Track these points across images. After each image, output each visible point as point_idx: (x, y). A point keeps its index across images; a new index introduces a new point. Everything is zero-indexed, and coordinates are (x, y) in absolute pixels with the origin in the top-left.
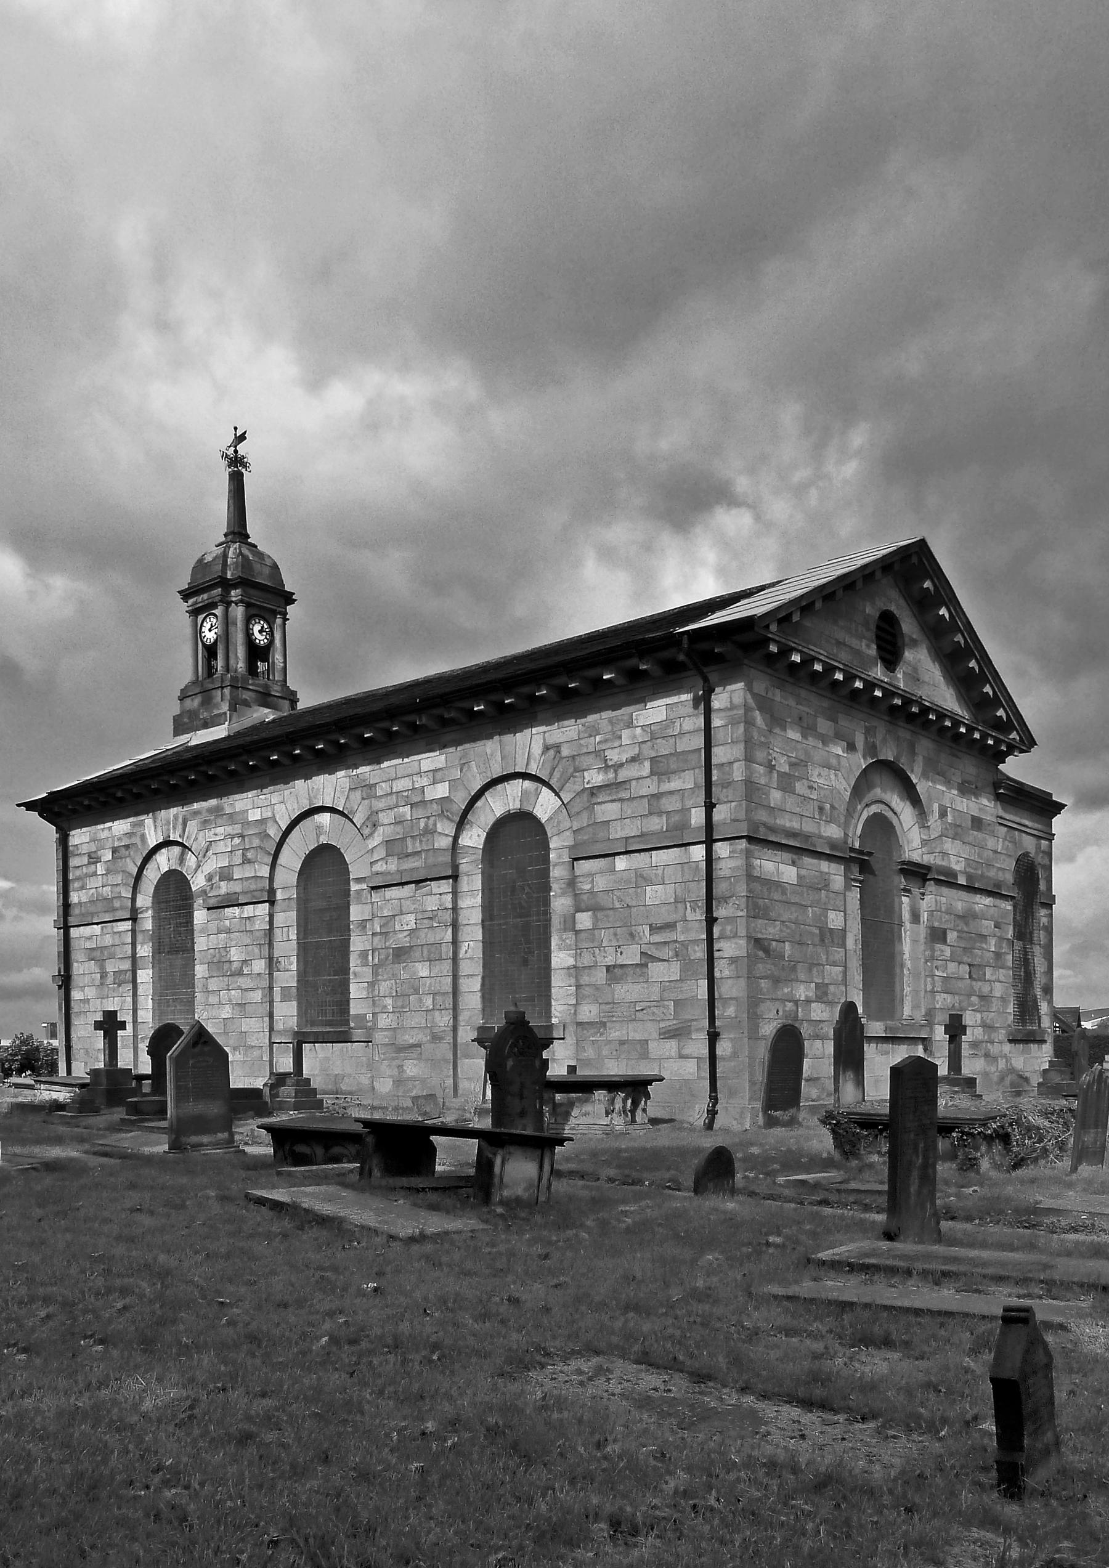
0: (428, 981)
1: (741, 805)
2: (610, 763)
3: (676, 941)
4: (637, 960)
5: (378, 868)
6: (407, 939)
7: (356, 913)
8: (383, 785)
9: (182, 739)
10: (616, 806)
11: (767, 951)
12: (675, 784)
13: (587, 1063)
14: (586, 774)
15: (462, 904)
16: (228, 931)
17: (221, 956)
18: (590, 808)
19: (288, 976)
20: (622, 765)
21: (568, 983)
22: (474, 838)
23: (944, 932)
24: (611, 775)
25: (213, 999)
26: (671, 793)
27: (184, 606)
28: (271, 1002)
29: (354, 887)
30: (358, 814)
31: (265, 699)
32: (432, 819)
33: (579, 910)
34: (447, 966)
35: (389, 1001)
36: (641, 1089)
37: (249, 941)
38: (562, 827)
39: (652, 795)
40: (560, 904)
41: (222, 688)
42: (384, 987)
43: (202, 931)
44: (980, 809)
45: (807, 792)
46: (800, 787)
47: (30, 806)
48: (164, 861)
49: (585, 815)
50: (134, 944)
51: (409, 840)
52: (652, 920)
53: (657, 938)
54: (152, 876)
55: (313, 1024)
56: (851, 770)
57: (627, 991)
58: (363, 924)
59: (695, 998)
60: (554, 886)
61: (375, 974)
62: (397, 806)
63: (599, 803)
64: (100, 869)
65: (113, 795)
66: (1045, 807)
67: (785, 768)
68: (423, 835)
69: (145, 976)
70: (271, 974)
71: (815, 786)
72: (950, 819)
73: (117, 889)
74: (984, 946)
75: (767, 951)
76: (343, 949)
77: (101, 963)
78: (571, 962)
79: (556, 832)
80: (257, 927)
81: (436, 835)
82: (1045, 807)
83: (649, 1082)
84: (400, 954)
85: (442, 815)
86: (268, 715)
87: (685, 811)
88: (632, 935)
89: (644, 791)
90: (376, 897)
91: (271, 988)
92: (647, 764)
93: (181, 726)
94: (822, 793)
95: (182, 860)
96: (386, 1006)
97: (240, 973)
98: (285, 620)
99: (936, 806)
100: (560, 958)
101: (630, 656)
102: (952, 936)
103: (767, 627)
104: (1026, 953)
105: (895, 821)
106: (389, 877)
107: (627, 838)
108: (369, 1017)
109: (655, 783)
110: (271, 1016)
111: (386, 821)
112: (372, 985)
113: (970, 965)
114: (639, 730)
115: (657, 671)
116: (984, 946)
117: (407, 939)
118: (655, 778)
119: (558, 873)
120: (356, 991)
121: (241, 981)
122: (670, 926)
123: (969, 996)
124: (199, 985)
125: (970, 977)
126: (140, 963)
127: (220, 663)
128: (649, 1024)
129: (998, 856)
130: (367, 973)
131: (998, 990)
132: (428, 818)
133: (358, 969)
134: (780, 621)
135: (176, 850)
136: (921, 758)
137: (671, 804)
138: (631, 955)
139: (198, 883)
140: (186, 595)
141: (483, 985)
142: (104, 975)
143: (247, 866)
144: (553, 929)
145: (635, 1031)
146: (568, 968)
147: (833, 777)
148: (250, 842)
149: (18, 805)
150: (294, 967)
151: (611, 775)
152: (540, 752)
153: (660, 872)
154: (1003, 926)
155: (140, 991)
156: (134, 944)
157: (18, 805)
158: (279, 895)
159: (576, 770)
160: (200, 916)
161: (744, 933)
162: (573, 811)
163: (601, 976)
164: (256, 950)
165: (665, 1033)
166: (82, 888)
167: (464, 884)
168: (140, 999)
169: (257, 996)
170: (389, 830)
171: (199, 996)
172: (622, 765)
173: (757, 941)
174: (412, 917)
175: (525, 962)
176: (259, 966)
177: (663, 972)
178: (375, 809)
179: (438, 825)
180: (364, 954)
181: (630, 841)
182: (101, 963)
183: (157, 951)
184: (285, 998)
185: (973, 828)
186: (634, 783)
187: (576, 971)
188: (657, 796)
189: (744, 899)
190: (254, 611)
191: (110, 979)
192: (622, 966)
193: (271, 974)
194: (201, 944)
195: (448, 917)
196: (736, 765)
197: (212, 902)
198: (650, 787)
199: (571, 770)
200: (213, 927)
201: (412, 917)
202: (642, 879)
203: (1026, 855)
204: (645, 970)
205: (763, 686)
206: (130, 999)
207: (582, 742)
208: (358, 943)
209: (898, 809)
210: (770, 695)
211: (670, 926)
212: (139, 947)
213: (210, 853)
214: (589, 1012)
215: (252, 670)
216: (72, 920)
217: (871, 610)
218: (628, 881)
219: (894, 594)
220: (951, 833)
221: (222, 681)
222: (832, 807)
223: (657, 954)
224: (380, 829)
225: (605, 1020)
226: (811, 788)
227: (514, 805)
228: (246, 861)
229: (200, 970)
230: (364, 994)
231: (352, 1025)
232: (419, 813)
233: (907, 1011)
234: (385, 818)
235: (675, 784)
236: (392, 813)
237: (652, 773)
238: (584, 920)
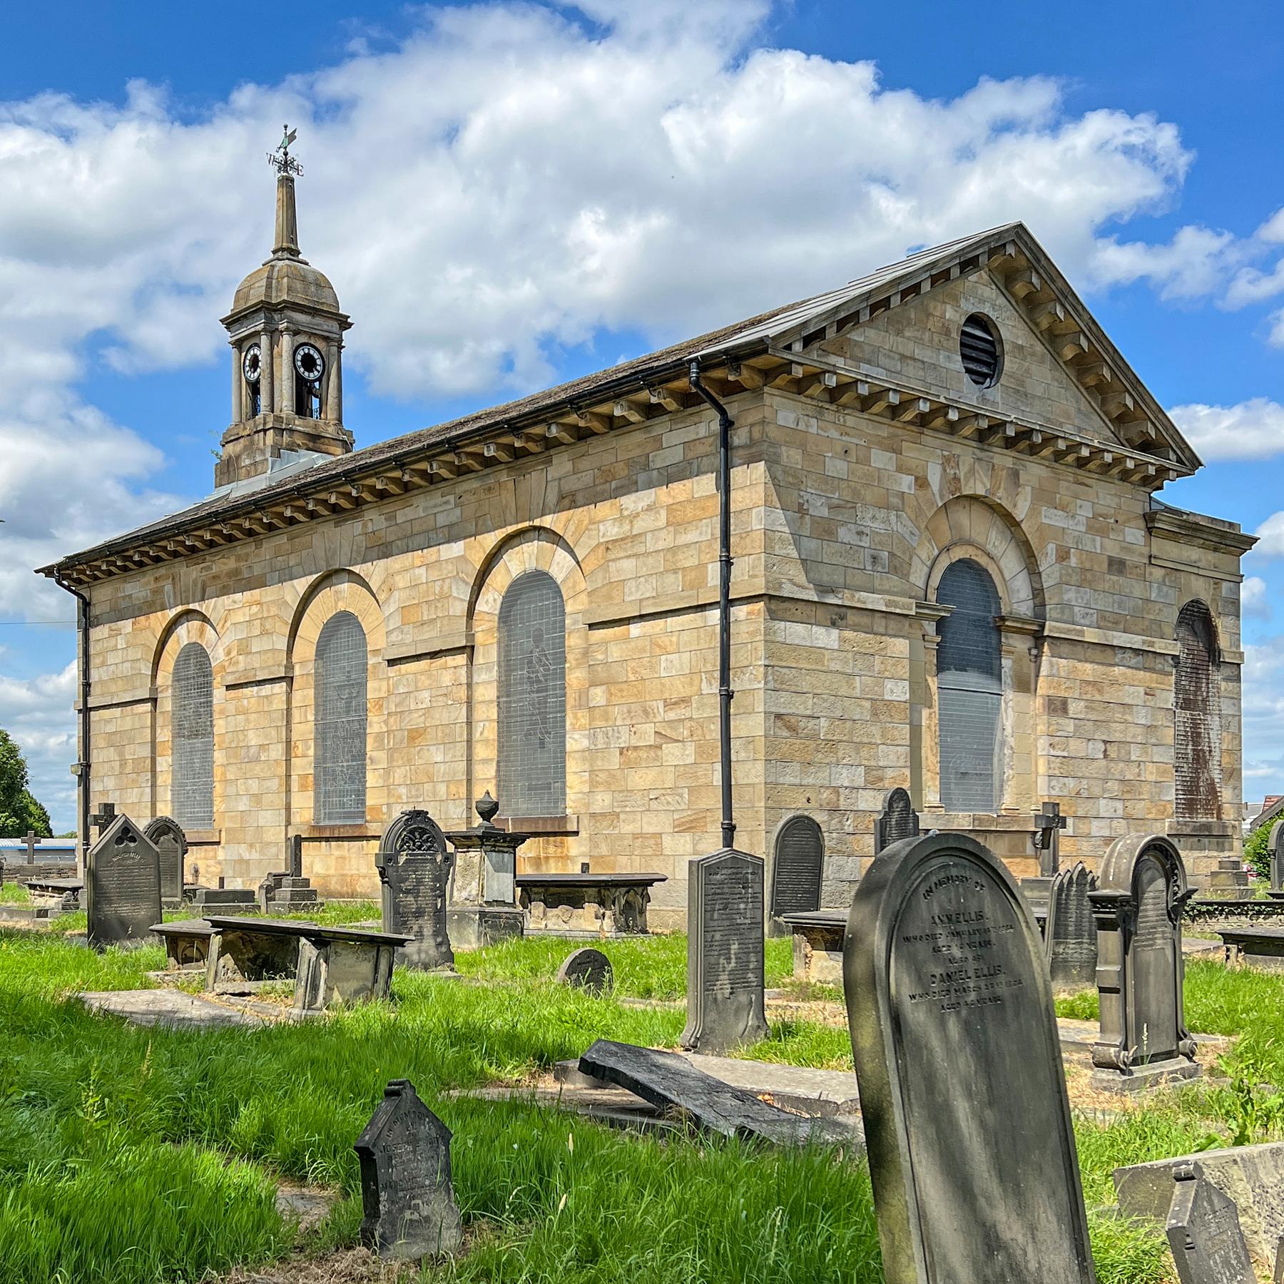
0: (442, 767)
1: (759, 559)
2: (626, 513)
3: (691, 719)
4: (651, 740)
5: (394, 637)
6: (422, 719)
7: (374, 689)
8: (399, 543)
9: (224, 490)
10: (632, 561)
11: (793, 729)
12: (691, 537)
13: (599, 859)
14: (601, 527)
15: (476, 679)
16: (246, 712)
17: (239, 741)
18: (604, 567)
19: (304, 765)
20: (638, 515)
21: (584, 768)
22: (490, 602)
23: (1064, 703)
24: (627, 527)
25: (231, 790)
26: (687, 546)
27: (227, 336)
28: (288, 791)
29: (372, 661)
30: (374, 577)
31: (315, 441)
32: (448, 581)
33: (594, 684)
34: (461, 749)
35: (403, 790)
36: (640, 890)
37: (266, 724)
38: (577, 590)
39: (668, 550)
40: (575, 678)
41: (265, 431)
42: (399, 774)
43: (222, 712)
44: (1122, 548)
45: (854, 539)
46: (844, 534)
47: (48, 571)
48: (184, 634)
49: (600, 575)
50: (153, 727)
51: (425, 607)
52: (666, 695)
53: (672, 715)
54: (173, 649)
55: (330, 816)
56: (920, 508)
57: (641, 779)
58: (380, 702)
59: (709, 785)
60: (569, 657)
61: (390, 759)
62: (413, 568)
63: (613, 560)
64: (121, 643)
65: (130, 558)
66: (1231, 542)
67: (825, 512)
68: (438, 600)
69: (164, 763)
70: (288, 761)
71: (867, 531)
72: (1073, 561)
73: (137, 665)
74: (1128, 717)
75: (793, 729)
76: (361, 735)
77: (120, 748)
78: (585, 743)
79: (572, 594)
80: (275, 707)
81: (450, 600)
82: (1231, 542)
83: (650, 883)
84: (414, 736)
85: (457, 578)
86: (319, 460)
87: (702, 566)
88: (646, 712)
89: (661, 545)
90: (393, 671)
91: (288, 776)
92: (663, 513)
93: (228, 470)
94: (877, 539)
95: (202, 632)
96: (400, 797)
97: (258, 760)
98: (340, 347)
99: (1051, 548)
100: (575, 741)
101: (640, 389)
102: (1075, 708)
103: (788, 348)
104: (1195, 725)
105: (992, 569)
106: (404, 649)
107: (641, 600)
108: (385, 809)
109: (671, 537)
110: (288, 808)
111: (401, 585)
112: (388, 772)
113: (1105, 742)
114: (655, 472)
115: (671, 404)
116: (1128, 717)
117: (422, 719)
118: (671, 529)
119: (574, 641)
120: (372, 779)
121: (258, 768)
122: (685, 701)
123: (1106, 781)
124: (218, 772)
125: (1106, 756)
126: (159, 749)
127: (263, 400)
128: (662, 816)
129: (1150, 605)
130: (382, 755)
131: (1150, 774)
132: (443, 580)
133: (374, 754)
134: (807, 341)
135: (196, 624)
136: (1028, 489)
137: (688, 560)
138: (647, 733)
139: (218, 656)
140: (230, 322)
141: (498, 771)
142: (123, 763)
143: (265, 638)
144: (568, 707)
145: (649, 823)
146: (583, 751)
147: (893, 518)
148: (268, 611)
149: (37, 572)
150: (311, 752)
151: (627, 527)
152: (555, 501)
153: (674, 639)
154: (1158, 692)
155: (159, 781)
156: (153, 727)
157: (37, 572)
158: (297, 671)
159: (592, 522)
160: (219, 694)
161: (762, 709)
162: (587, 569)
163: (615, 761)
164: (273, 732)
165: (679, 826)
166: (103, 664)
167: (479, 658)
168: (159, 790)
169: (274, 784)
170: (404, 595)
171: (218, 789)
172: (638, 515)
173: (778, 716)
174: (426, 694)
175: (542, 744)
176: (277, 752)
177: (674, 754)
178: (391, 571)
179: (454, 588)
180: (379, 736)
181: (644, 603)
182: (120, 748)
183: (177, 735)
184: (303, 788)
185: (1110, 571)
186: (649, 535)
187: (590, 754)
188: (674, 550)
189: (762, 669)
190: (302, 339)
191: (129, 769)
192: (636, 748)
193: (288, 761)
194: (220, 726)
195: (463, 693)
196: (754, 511)
197: (231, 680)
198: (666, 540)
199: (586, 522)
200: (231, 708)
201: (426, 694)
202: (656, 647)
203: (1196, 602)
204: (659, 753)
205: (792, 416)
206: (148, 790)
207: (598, 489)
208: (375, 724)
209: (996, 552)
210: (802, 427)
211: (685, 701)
212: (158, 731)
213: (228, 624)
214: (602, 801)
215: (301, 408)
216: (92, 702)
217: (954, 315)
218: (643, 650)
219: (990, 292)
220: (1075, 579)
221: (265, 424)
222: (892, 554)
223: (668, 732)
224: (396, 594)
225: (618, 810)
226: (860, 533)
227: (531, 566)
228: (265, 633)
229: (219, 756)
230: (381, 783)
231: (368, 818)
232: (434, 575)
233: (1008, 800)
234: (401, 582)
235: (691, 537)
236: (407, 576)
237: (668, 524)
238: (598, 696)
